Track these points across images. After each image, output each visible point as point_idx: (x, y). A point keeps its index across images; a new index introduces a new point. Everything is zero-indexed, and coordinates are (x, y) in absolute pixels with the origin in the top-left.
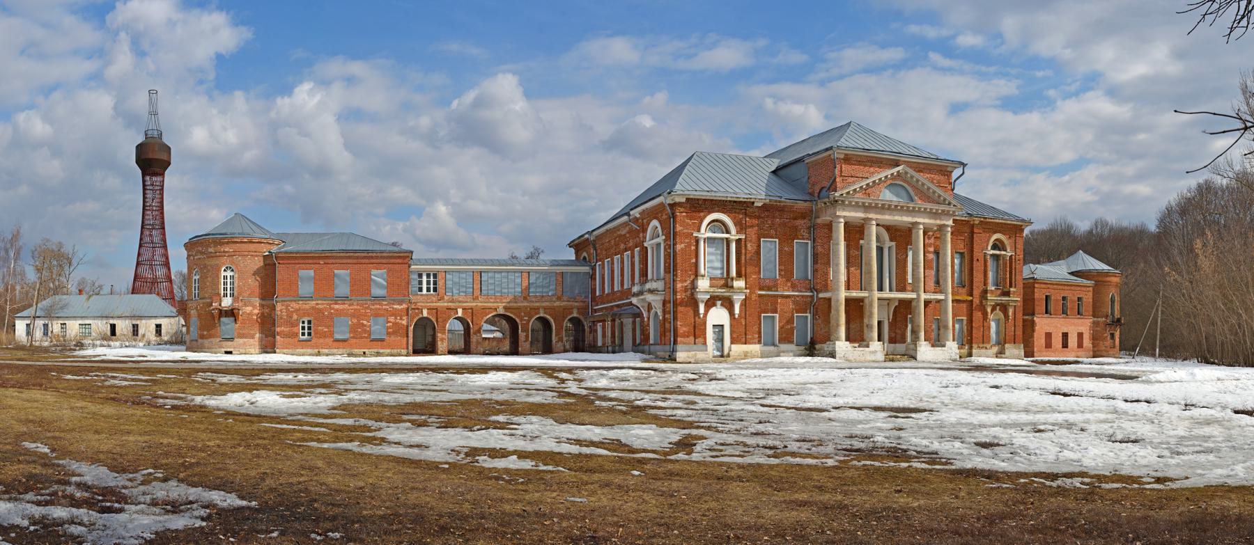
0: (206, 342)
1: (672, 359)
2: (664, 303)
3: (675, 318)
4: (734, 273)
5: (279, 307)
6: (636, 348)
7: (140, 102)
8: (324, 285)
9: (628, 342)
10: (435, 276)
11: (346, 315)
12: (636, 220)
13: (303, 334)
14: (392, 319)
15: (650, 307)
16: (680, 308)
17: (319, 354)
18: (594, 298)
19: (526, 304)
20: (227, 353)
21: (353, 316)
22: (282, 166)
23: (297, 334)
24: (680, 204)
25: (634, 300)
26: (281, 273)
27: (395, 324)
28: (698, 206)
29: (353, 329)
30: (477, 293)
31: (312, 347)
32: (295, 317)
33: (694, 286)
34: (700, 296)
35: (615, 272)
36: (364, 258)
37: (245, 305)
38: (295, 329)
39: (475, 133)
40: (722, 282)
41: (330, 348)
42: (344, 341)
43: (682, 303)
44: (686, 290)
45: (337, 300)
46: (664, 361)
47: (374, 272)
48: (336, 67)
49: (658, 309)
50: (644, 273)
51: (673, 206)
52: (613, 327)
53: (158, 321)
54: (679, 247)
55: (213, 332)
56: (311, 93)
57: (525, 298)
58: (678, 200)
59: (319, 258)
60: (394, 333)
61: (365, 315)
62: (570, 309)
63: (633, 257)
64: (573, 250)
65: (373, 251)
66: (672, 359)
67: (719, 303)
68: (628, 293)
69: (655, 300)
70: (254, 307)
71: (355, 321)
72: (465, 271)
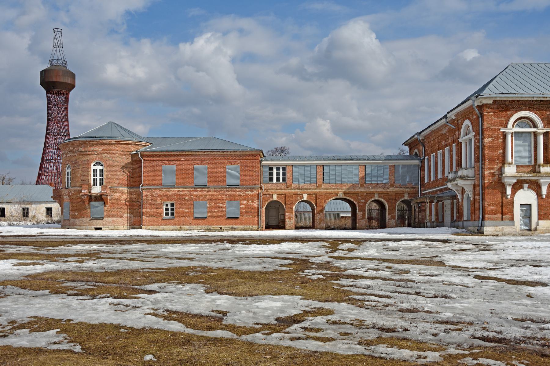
0: (77, 221)
1: (480, 232)
2: (474, 187)
3: (483, 199)
4: (541, 160)
5: (144, 193)
6: (454, 223)
7: (48, 45)
8: (185, 177)
9: (448, 219)
10: (284, 169)
11: (205, 199)
12: (453, 121)
13: (167, 214)
14: (245, 202)
15: (463, 191)
16: (487, 191)
17: (180, 229)
18: (423, 185)
19: (362, 190)
20: (96, 229)
21: (211, 200)
22: (186, 97)
23: (161, 214)
24: (487, 106)
25: (449, 185)
26: (146, 167)
27: (247, 206)
28: (505, 107)
29: (211, 210)
30: (320, 181)
31: (175, 224)
32: (159, 201)
33: (501, 172)
34: (506, 181)
35: (438, 163)
36: (219, 156)
37: (114, 192)
38: (159, 211)
39: (337, 67)
40: (530, 168)
41: (190, 224)
42: (203, 219)
43: (490, 186)
44: (493, 175)
45: (196, 187)
46: (472, 234)
47: (229, 166)
48: (226, 22)
49: (469, 192)
50: (459, 164)
51: (480, 107)
52: (437, 207)
53: (49, 206)
54: (486, 141)
55: (83, 213)
56: (208, 41)
57: (362, 186)
58: (485, 102)
59: (180, 156)
60: (247, 213)
61: (221, 199)
62: (402, 194)
63: (451, 150)
64: (407, 148)
65: (227, 151)
66: (480, 232)
67: (526, 186)
68: (445, 180)
69: (467, 185)
70: (123, 193)
71: (212, 204)
72: (310, 165)
